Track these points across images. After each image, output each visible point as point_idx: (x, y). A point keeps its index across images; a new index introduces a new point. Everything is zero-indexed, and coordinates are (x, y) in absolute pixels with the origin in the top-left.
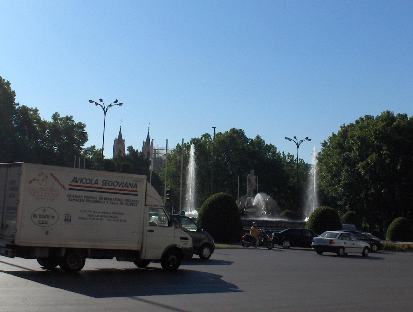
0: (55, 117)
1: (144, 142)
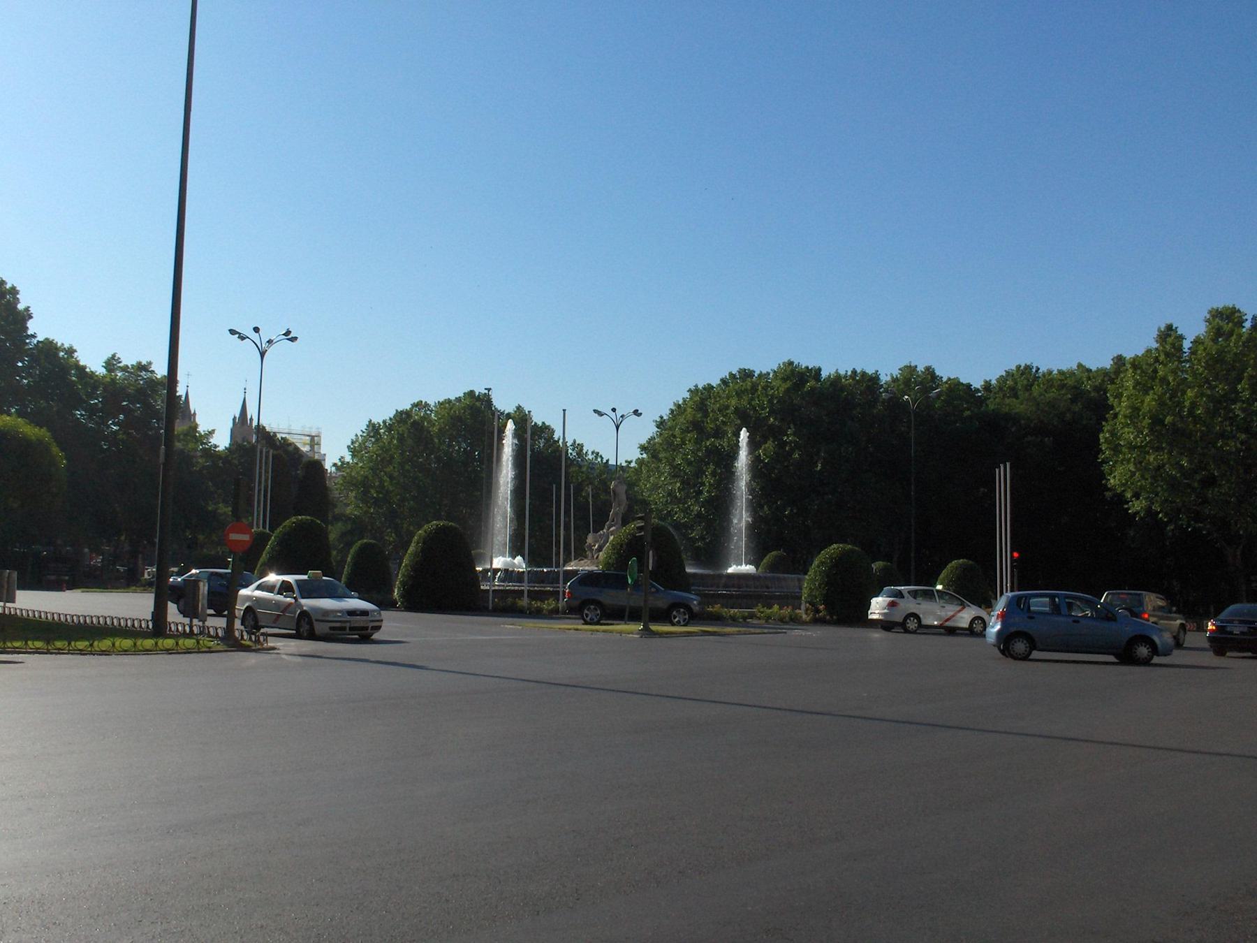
0: (111, 364)
1: (235, 418)
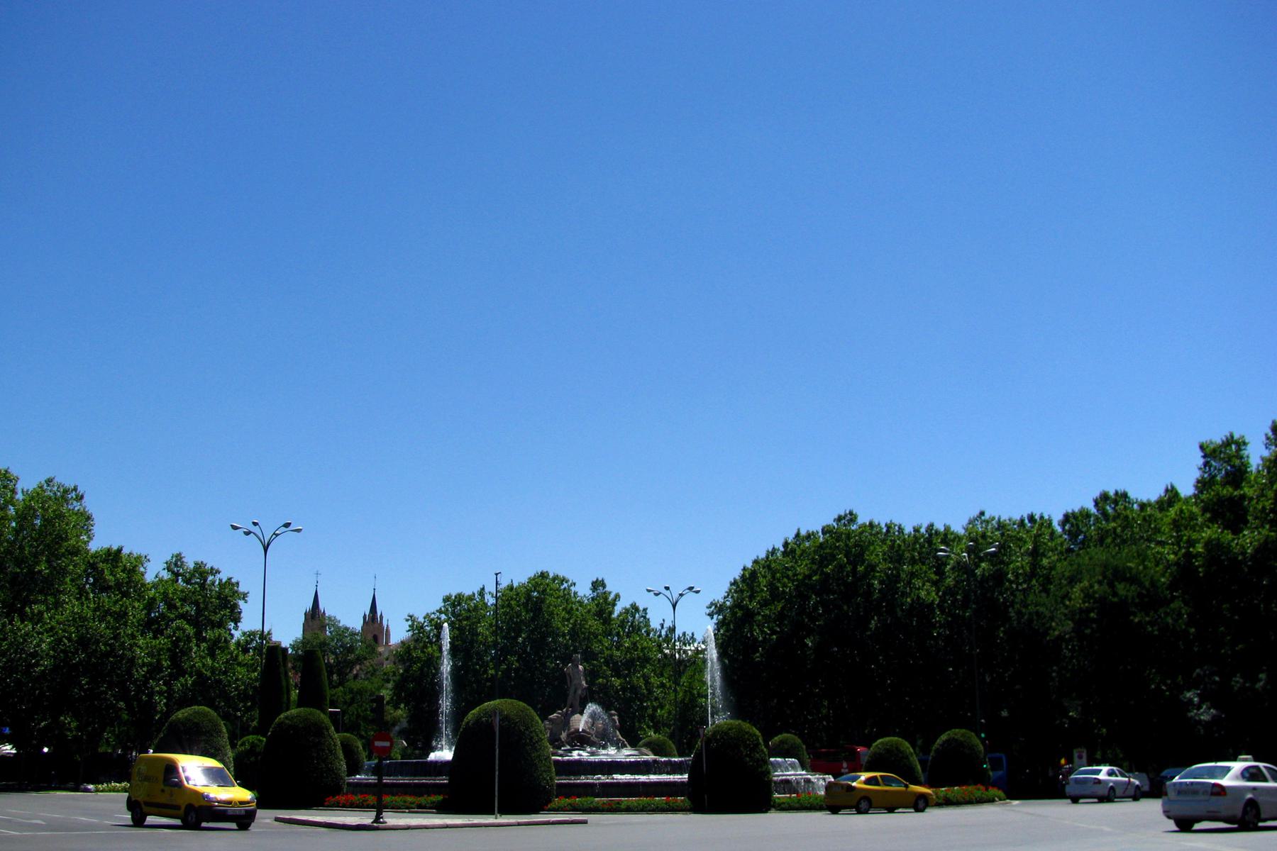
0: (175, 565)
1: (365, 615)
